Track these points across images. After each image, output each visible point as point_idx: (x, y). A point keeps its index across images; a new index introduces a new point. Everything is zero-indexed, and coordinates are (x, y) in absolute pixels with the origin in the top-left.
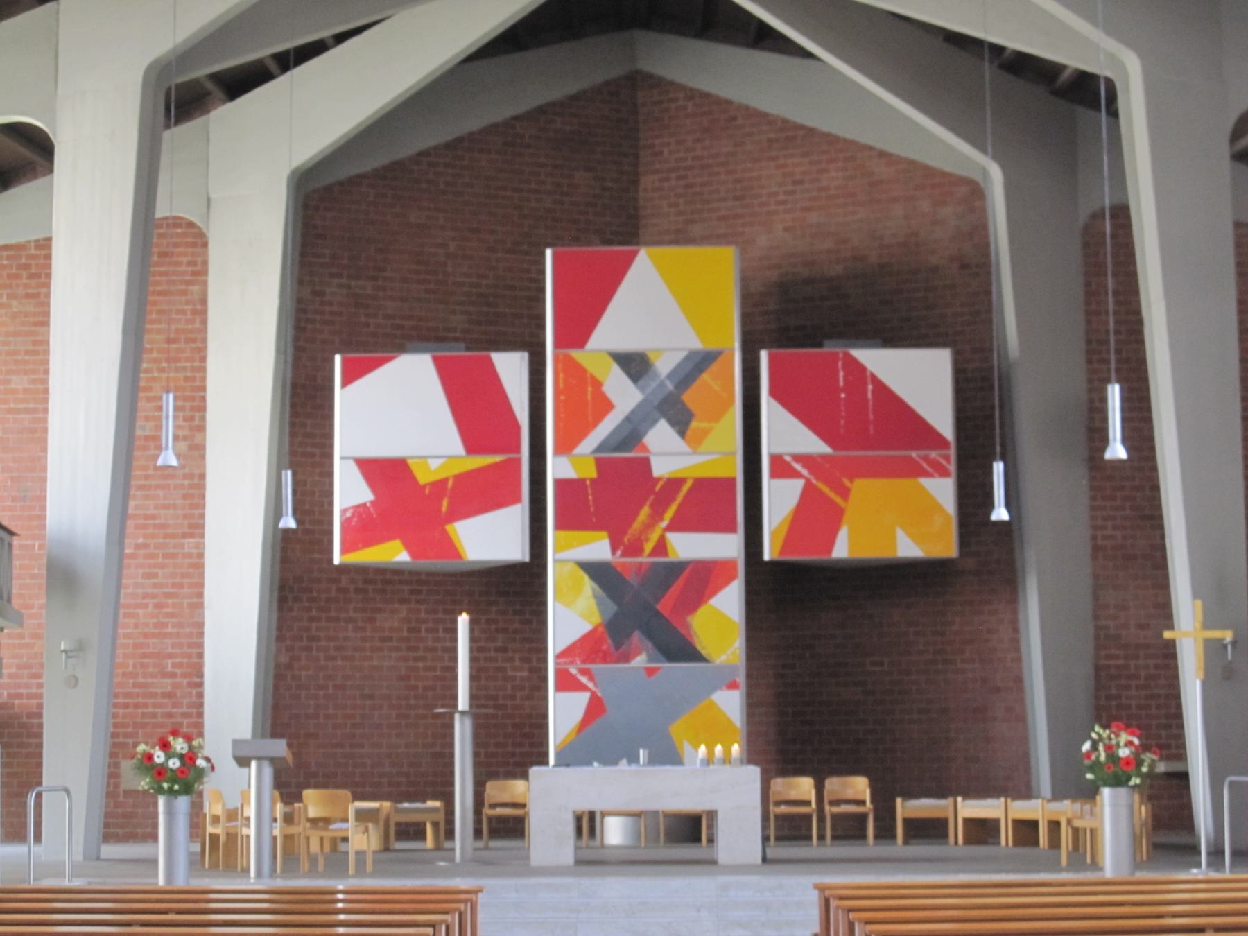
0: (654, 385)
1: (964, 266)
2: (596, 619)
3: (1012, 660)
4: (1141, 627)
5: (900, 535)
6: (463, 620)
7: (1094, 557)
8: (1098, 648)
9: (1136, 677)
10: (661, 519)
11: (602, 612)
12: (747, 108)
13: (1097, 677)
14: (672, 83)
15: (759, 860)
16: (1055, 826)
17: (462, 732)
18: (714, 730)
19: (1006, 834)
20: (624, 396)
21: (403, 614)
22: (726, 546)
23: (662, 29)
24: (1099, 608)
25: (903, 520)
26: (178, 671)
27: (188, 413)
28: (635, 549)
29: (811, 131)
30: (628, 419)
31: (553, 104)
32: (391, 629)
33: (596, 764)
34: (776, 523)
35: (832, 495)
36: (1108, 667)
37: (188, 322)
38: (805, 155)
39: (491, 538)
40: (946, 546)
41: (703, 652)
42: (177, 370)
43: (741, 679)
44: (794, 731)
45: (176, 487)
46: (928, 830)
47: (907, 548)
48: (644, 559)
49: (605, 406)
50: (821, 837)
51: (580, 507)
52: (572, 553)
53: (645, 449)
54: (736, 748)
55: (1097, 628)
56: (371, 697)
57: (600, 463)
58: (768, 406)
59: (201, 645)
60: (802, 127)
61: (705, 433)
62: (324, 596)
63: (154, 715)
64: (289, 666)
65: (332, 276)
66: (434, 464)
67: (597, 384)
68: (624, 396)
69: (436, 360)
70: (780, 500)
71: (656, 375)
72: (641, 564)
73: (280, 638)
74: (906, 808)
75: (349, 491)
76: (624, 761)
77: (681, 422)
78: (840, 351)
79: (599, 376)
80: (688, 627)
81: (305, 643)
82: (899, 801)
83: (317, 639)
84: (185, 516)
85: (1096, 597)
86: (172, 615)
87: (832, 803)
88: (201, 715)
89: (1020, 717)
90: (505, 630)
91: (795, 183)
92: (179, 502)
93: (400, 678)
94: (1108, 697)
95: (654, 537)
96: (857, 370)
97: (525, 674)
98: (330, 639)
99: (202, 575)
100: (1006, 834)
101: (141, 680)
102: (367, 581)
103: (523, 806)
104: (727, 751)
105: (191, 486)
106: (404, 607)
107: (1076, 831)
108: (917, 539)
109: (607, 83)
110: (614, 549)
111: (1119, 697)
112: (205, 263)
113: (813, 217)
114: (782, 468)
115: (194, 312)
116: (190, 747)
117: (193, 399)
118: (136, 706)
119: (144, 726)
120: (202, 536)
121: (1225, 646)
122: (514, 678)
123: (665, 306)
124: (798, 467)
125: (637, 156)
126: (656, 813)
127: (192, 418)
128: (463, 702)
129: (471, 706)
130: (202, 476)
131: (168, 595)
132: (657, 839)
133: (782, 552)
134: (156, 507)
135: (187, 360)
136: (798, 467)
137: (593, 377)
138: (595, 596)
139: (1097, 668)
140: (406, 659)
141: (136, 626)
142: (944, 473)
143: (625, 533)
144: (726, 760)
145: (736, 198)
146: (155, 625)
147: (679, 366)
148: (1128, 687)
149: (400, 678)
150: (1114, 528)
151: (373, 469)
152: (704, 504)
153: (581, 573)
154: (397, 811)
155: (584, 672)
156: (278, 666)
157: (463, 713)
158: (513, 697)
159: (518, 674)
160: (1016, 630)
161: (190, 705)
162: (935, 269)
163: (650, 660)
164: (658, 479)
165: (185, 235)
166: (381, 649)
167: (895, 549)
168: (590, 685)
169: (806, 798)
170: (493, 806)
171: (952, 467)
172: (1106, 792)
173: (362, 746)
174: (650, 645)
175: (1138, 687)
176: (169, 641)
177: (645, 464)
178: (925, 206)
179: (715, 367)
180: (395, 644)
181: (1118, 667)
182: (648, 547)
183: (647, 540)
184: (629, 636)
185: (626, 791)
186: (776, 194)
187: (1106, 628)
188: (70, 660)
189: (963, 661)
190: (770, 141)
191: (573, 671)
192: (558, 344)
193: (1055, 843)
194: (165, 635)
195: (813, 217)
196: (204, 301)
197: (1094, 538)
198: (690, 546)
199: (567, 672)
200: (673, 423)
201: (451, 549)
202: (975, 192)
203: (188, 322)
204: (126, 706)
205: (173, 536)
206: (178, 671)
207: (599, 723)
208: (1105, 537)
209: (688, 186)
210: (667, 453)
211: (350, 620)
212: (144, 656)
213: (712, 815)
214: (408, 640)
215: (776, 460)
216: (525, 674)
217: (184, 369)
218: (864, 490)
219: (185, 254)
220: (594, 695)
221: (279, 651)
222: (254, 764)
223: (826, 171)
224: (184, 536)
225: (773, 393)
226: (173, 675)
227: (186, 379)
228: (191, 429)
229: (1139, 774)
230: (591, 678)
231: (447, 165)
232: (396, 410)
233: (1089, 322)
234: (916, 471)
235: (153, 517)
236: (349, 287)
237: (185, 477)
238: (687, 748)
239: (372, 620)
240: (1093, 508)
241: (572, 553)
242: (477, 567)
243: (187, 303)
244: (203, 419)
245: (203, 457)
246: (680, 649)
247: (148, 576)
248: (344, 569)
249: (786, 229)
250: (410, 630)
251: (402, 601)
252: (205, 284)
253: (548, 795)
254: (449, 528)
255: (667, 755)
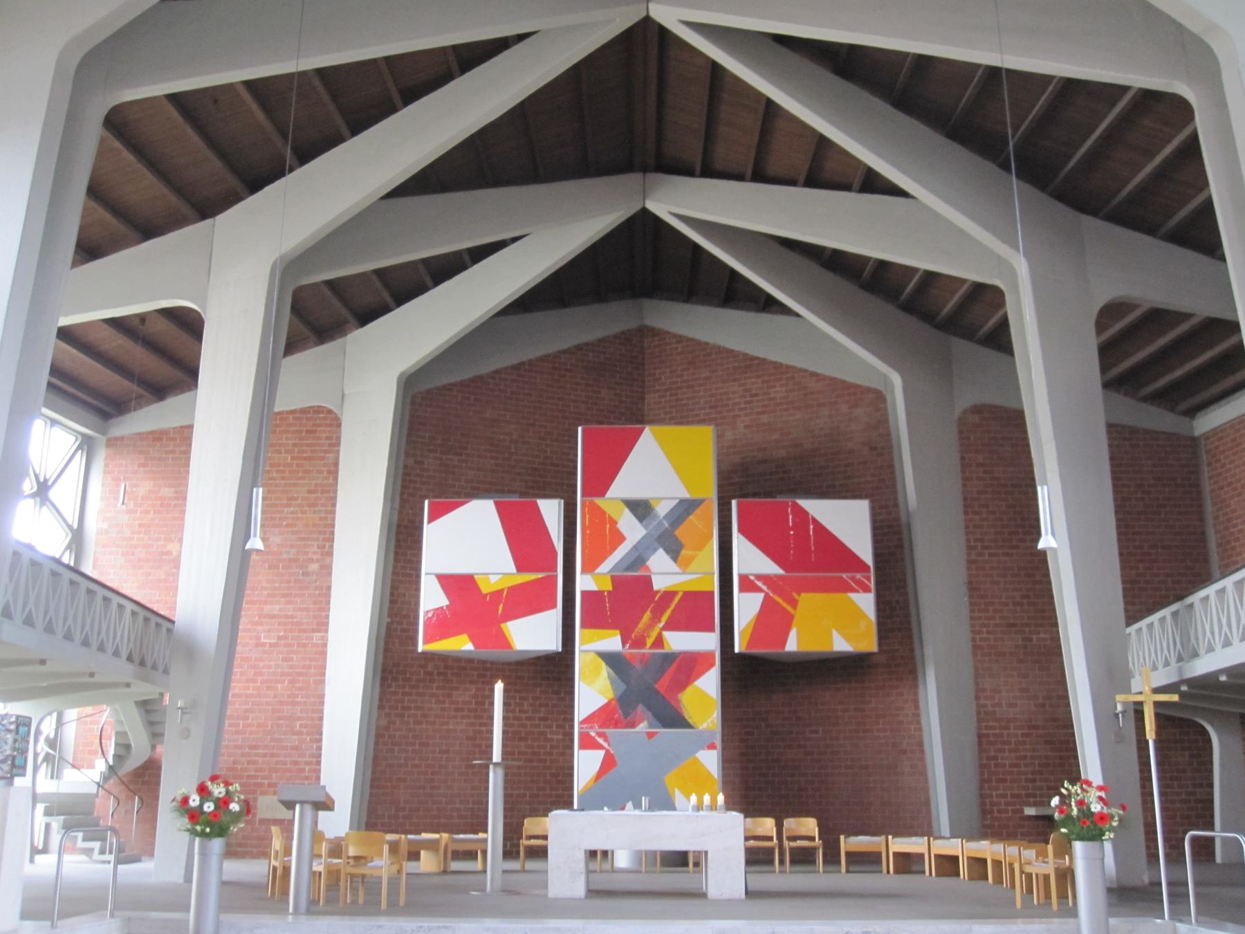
0: (655, 523)
1: (872, 449)
2: (610, 695)
3: (916, 730)
4: (1011, 705)
5: (835, 635)
6: (499, 687)
7: (974, 654)
8: (979, 721)
9: (1008, 743)
10: (660, 621)
11: (614, 689)
12: (719, 347)
13: (980, 743)
14: (668, 333)
15: (743, 896)
16: (997, 864)
17: (495, 781)
18: (697, 782)
19: (929, 866)
20: (632, 530)
21: (473, 692)
22: (708, 642)
23: (661, 298)
24: (979, 692)
25: (838, 624)
26: (304, 730)
27: (321, 543)
28: (639, 643)
29: (763, 361)
30: (635, 547)
31: (587, 344)
32: (463, 702)
33: (1041, 545)
34: (743, 625)
35: (784, 605)
36: (988, 735)
37: (324, 478)
38: (758, 377)
39: (534, 634)
40: (868, 643)
41: (690, 721)
42: (314, 512)
43: (718, 743)
44: (755, 783)
45: (309, 596)
46: (866, 861)
47: (841, 645)
48: (646, 651)
49: (619, 538)
50: (782, 862)
51: (600, 612)
52: (595, 644)
53: (647, 569)
54: (721, 798)
55: (978, 706)
56: (447, 752)
57: (615, 580)
58: (739, 543)
59: (322, 711)
60: (758, 358)
61: (692, 558)
62: (415, 677)
63: (285, 763)
64: (387, 728)
65: (430, 451)
66: (493, 579)
67: (614, 523)
68: (632, 530)
69: (497, 504)
70: (746, 607)
71: (656, 516)
72: (644, 654)
73: (381, 707)
74: (848, 843)
75: (431, 598)
76: (629, 805)
77: (674, 552)
78: (789, 501)
79: (614, 516)
80: (678, 702)
81: (399, 711)
82: (842, 837)
83: (409, 708)
84: (315, 617)
85: (977, 684)
86: (301, 689)
87: (791, 839)
88: (319, 763)
89: (921, 772)
90: (547, 706)
91: (752, 396)
92: (311, 606)
93: (468, 738)
94: (989, 758)
95: (654, 634)
96: (802, 514)
97: (560, 737)
98: (417, 708)
99: (325, 660)
100: (929, 866)
101: (276, 736)
102: (447, 667)
103: (545, 838)
104: (714, 799)
105: (320, 595)
106: (473, 687)
107: (1029, 876)
108: (848, 639)
109: (623, 333)
110: (624, 643)
111: (996, 758)
112: (339, 438)
113: (765, 419)
114: (748, 585)
115: (329, 472)
116: (227, 792)
117: (325, 533)
118: (272, 755)
119: (276, 771)
120: (327, 631)
121: (1117, 715)
122: (552, 740)
123: (661, 468)
124: (759, 584)
125: (643, 382)
126: (654, 852)
127: (324, 547)
128: (497, 755)
129: (503, 759)
130: (329, 588)
131: (300, 674)
132: (655, 865)
133: (748, 647)
134: (294, 610)
135: (323, 505)
136: (759, 584)
137: (611, 518)
138: (610, 678)
139: (980, 736)
140: (472, 724)
141: (275, 696)
142: (866, 589)
143: (632, 631)
144: (713, 807)
145: (711, 407)
146: (289, 696)
147: (672, 510)
148: (1004, 751)
149: (468, 738)
150: (988, 632)
151: (450, 583)
152: (691, 610)
153: (600, 660)
154: (455, 841)
155: (600, 735)
156: (378, 728)
157: (496, 764)
158: (551, 754)
159: (555, 737)
160: (917, 707)
161: (312, 756)
162: (851, 452)
163: (651, 726)
164: (657, 592)
165: (325, 418)
166: (455, 717)
167: (832, 645)
168: (605, 745)
169: (769, 834)
170: (530, 837)
171: (872, 585)
172: (1078, 846)
173: (439, 788)
174: (650, 714)
175: (1010, 751)
176: (299, 708)
177: (647, 581)
178: (844, 408)
179: (698, 511)
180: (466, 713)
181: (995, 735)
182: (649, 642)
183: (649, 636)
184: (635, 708)
185: (629, 833)
186: (738, 403)
187: (985, 706)
188: (186, 717)
189: (878, 730)
190: (734, 368)
191: (593, 734)
192: (583, 495)
193: (998, 879)
194: (297, 703)
195: (765, 419)
196: (336, 464)
197: (973, 640)
198: (680, 641)
199: (588, 735)
200: (668, 551)
201: (505, 642)
202: (878, 399)
203: (324, 478)
204: (265, 755)
205: (305, 631)
206: (304, 730)
207: (612, 774)
208: (981, 640)
209: (677, 400)
210: (665, 573)
211: (432, 695)
212: (280, 718)
213: (706, 853)
214: (476, 710)
215: (744, 579)
216: (560, 737)
217: (320, 511)
218: (808, 602)
219: (324, 432)
220: (607, 752)
221: (379, 716)
222: (298, 807)
223: (775, 387)
224: (313, 631)
225: (741, 530)
226: (300, 733)
227: (321, 519)
228: (322, 554)
229: (1111, 829)
230: (606, 740)
231: (513, 381)
232: (468, 540)
233: (964, 486)
234: (847, 588)
235: (292, 617)
236: (441, 459)
237: (316, 588)
238: (678, 797)
239: (450, 696)
240: (972, 618)
241: (595, 644)
242: (526, 656)
243: (325, 465)
244: (331, 547)
245: (330, 574)
246: (674, 719)
247: (284, 660)
248: (428, 656)
249: (746, 427)
250: (476, 703)
251: (471, 682)
252: (338, 452)
253: (566, 833)
254: (503, 625)
255: (664, 802)
